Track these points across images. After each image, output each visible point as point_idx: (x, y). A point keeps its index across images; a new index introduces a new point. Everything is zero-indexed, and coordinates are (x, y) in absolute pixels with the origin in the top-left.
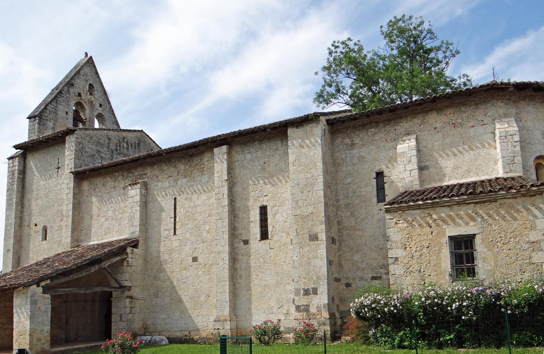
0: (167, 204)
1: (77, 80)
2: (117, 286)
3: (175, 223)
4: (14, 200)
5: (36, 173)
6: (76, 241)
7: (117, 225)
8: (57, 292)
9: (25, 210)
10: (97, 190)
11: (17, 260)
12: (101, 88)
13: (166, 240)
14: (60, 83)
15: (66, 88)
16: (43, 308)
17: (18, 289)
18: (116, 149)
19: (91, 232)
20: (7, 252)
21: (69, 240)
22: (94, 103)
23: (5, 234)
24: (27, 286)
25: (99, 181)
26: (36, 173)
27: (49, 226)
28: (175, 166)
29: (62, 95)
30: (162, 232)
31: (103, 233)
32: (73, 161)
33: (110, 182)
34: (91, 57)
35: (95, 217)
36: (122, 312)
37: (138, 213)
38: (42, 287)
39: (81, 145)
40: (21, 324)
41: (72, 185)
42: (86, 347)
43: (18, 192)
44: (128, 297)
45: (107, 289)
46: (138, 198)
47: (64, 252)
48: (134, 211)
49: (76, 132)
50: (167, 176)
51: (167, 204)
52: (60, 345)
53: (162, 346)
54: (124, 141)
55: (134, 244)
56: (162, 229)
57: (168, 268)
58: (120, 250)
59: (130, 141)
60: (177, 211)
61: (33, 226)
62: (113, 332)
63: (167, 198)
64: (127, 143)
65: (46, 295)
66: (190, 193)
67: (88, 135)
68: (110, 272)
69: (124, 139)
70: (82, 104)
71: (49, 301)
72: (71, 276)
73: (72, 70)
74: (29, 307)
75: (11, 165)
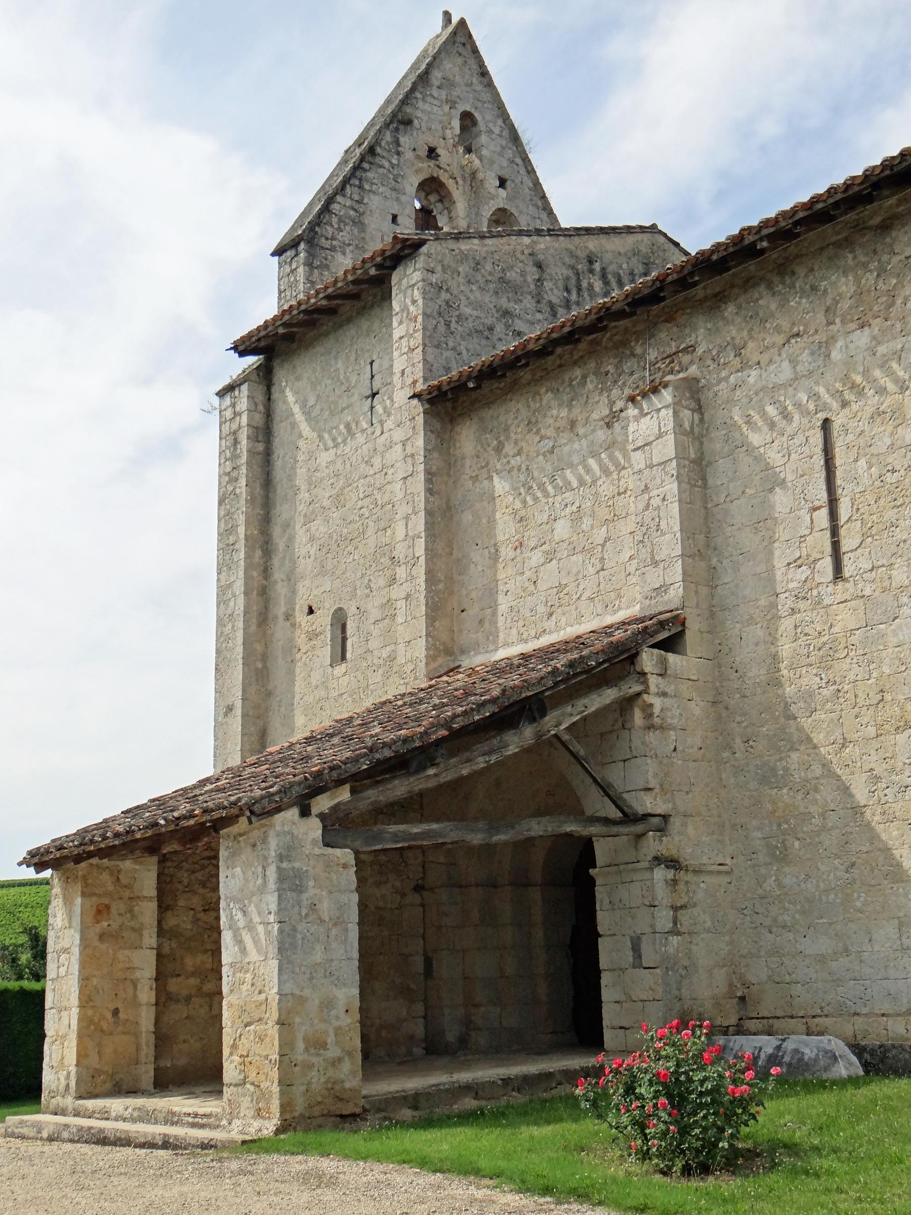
0: (790, 453)
1: (420, 104)
2: (615, 814)
3: (835, 531)
4: (241, 530)
5: (305, 428)
6: (445, 651)
7: (592, 570)
8: (377, 838)
9: (276, 562)
10: (509, 449)
11: (258, 733)
12: (500, 122)
13: (802, 605)
14: (371, 124)
15: (388, 137)
16: (326, 908)
17: (234, 829)
18: (568, 301)
19: (494, 614)
20: (226, 715)
21: (420, 649)
22: (480, 176)
23: (218, 652)
24: (262, 811)
25: (513, 413)
26: (305, 428)
27: (351, 611)
28: (814, 288)
29: (377, 160)
30: (779, 575)
31: (541, 609)
32: (418, 355)
33: (554, 410)
34: (462, 23)
35: (506, 552)
36: (641, 925)
37: (675, 508)
38: (322, 816)
39: (444, 296)
40: (249, 976)
41: (420, 442)
42: (506, 1081)
43: (251, 501)
44: (658, 860)
45: (572, 828)
46: (667, 448)
47: (403, 695)
48: (655, 502)
49: (424, 249)
50: (780, 339)
51: (790, 453)
52: (405, 1062)
53: (823, 1085)
54: (591, 271)
55: (668, 634)
56: (779, 563)
57: (819, 727)
58: (613, 662)
59: (612, 268)
60: (839, 474)
61: (301, 617)
62: (610, 1015)
63: (790, 430)
64: (604, 276)
65: (338, 852)
66: (891, 387)
67: (464, 257)
68: (582, 753)
69: (591, 262)
70: (441, 185)
71: (350, 877)
72: (431, 772)
73: (404, 77)
74: (272, 901)
75: (229, 414)
